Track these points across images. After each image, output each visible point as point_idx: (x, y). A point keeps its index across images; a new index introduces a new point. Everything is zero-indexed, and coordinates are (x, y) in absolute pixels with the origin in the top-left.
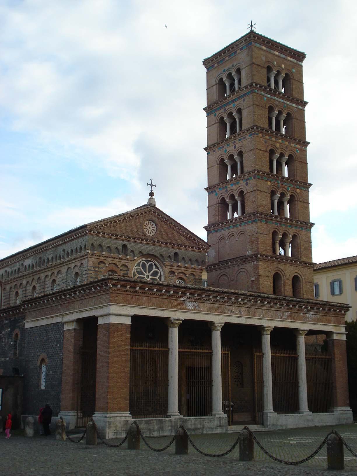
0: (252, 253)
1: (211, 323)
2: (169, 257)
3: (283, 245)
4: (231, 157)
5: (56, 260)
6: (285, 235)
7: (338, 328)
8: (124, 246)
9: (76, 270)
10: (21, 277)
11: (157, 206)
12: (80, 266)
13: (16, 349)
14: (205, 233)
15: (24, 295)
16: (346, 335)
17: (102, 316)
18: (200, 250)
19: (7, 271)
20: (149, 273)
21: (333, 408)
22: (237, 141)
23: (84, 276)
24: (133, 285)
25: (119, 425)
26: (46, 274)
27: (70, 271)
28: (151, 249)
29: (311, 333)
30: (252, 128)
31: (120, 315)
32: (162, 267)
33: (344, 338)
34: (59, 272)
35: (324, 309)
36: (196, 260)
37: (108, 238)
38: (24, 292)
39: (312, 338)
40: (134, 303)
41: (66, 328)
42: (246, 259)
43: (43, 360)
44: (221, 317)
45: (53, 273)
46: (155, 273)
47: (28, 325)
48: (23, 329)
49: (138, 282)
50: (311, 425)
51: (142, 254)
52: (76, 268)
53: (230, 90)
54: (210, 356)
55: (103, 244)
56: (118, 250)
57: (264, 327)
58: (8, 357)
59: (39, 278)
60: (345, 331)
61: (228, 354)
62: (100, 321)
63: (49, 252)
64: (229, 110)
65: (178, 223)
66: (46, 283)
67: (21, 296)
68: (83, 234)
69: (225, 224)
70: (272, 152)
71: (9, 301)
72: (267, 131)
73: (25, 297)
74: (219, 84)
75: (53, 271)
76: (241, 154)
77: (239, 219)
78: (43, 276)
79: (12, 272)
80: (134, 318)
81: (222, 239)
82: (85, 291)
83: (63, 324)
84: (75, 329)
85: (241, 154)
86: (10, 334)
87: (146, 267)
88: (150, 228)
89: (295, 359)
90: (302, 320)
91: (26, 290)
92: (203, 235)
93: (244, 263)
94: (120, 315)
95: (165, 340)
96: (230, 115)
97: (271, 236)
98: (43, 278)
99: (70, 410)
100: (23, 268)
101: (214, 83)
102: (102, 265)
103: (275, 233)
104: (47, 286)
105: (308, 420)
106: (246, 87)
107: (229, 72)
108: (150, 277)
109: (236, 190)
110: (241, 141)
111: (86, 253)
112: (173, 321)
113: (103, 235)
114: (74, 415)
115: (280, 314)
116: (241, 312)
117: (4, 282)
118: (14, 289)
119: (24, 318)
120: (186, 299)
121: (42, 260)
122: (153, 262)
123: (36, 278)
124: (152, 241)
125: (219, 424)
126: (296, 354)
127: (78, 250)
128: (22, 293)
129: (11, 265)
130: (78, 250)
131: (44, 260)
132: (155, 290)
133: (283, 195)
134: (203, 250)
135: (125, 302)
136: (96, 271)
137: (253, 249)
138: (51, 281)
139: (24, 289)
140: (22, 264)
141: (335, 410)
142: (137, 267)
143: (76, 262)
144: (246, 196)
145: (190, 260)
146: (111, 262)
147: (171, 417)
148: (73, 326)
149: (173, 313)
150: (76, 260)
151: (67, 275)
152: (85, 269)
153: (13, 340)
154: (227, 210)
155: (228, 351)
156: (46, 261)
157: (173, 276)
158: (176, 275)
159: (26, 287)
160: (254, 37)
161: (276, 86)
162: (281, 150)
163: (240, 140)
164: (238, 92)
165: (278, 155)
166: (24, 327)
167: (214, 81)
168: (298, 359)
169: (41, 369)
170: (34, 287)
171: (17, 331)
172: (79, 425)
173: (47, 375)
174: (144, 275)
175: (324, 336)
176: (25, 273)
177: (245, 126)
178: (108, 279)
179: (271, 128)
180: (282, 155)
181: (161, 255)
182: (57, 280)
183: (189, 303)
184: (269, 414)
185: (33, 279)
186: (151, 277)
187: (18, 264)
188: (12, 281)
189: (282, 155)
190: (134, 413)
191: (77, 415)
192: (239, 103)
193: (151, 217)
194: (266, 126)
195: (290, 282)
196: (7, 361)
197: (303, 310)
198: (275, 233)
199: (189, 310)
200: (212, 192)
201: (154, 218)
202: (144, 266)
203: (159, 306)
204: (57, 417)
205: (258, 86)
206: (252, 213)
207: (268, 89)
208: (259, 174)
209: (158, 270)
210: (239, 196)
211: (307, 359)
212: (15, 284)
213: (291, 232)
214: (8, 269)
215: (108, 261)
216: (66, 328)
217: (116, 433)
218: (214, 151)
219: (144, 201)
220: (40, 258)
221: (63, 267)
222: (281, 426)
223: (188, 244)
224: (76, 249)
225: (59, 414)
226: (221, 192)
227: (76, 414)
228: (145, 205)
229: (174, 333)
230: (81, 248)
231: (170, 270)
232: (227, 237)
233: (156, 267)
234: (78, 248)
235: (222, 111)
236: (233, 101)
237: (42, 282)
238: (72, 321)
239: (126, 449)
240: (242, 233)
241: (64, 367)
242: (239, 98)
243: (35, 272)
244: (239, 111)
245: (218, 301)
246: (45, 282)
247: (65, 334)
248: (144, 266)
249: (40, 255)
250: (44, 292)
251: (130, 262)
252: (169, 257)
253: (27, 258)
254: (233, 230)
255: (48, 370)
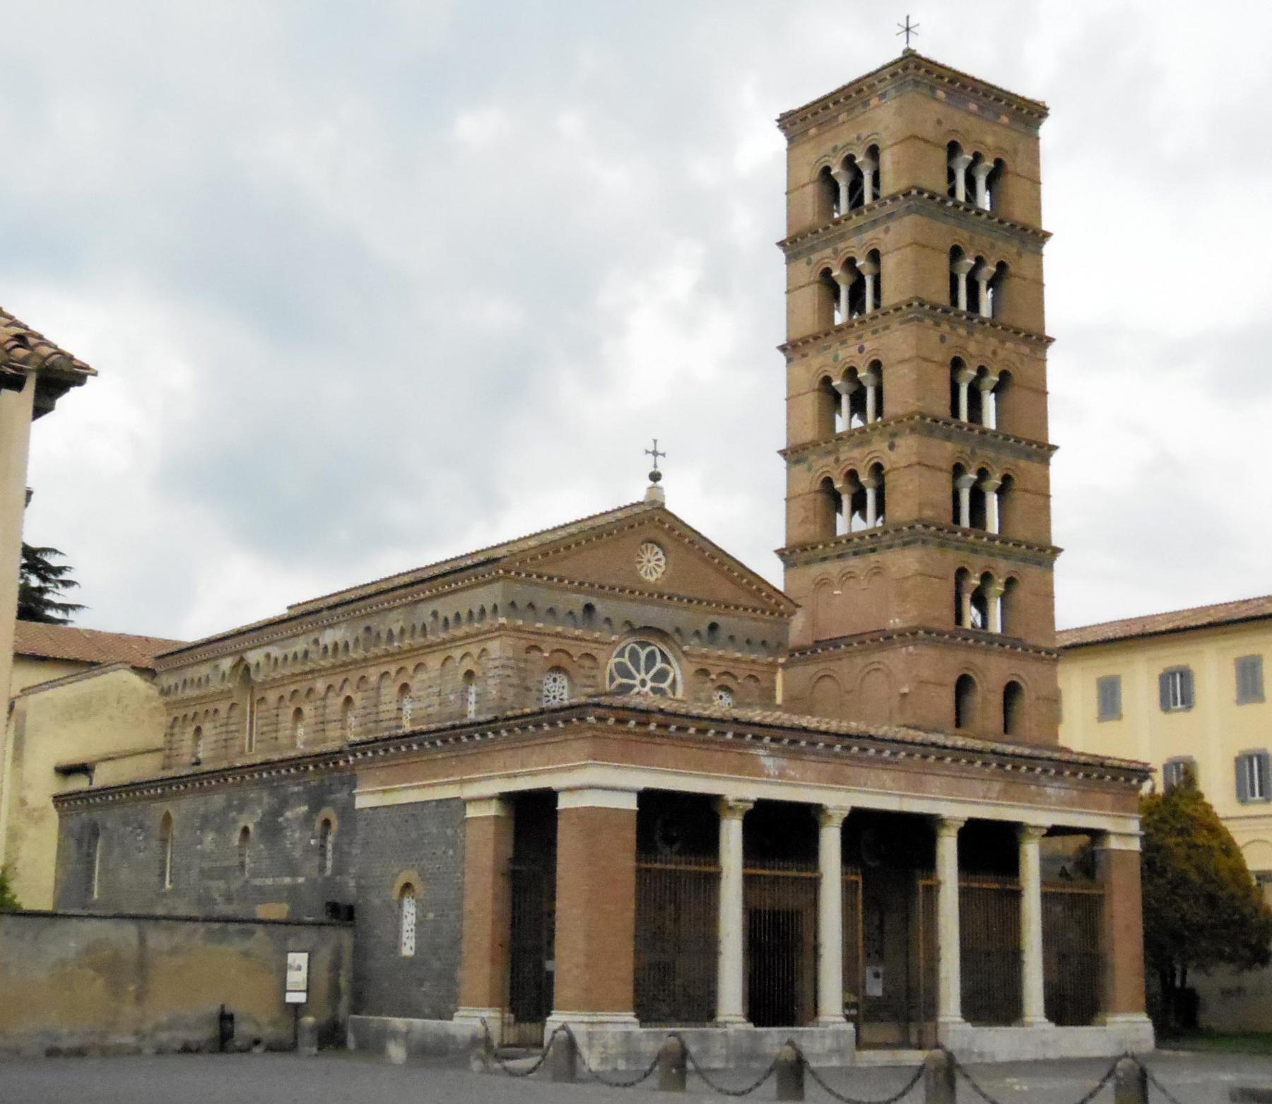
0: (905, 625)
1: (819, 808)
2: (697, 633)
3: (980, 601)
4: (851, 373)
5: (412, 635)
6: (986, 577)
7: (1121, 821)
8: (589, 608)
9: (468, 664)
10: (312, 671)
11: (669, 506)
12: (480, 657)
13: (323, 855)
14: (779, 565)
15: (321, 719)
16: (1143, 839)
17: (569, 790)
18: (772, 618)
19: (273, 656)
20: (647, 672)
21: (1107, 1016)
22: (867, 335)
23: (491, 682)
24: (643, 718)
25: (611, 1042)
26: (383, 669)
27: (449, 663)
28: (652, 614)
29: (1055, 831)
30: (909, 305)
31: (613, 789)
32: (678, 660)
33: (1135, 845)
34: (419, 667)
35: (1087, 776)
36: (764, 643)
37: (550, 588)
38: (320, 711)
39: (1057, 843)
40: (644, 762)
41: (471, 812)
42: (888, 638)
43: (407, 887)
44: (842, 794)
45: (401, 670)
46: (661, 675)
47: (364, 800)
48: (348, 812)
49: (653, 712)
50: (1051, 1054)
51: (632, 629)
52: (468, 659)
53: (851, 196)
54: (814, 885)
55: (538, 604)
56: (574, 618)
57: (942, 820)
58: (302, 876)
59: (363, 677)
60: (1138, 828)
61: (857, 882)
62: (563, 803)
63: (394, 615)
64: (846, 250)
65: (721, 550)
66: (383, 691)
67: (312, 721)
68: (490, 578)
69: (832, 545)
70: (957, 365)
71: (276, 731)
72: (945, 311)
73: (323, 723)
74: (818, 180)
75: (402, 664)
76: (876, 367)
77: (872, 536)
78: (373, 674)
79: (286, 658)
80: (648, 798)
81: (823, 583)
82: (524, 728)
83: (464, 803)
84: (496, 817)
85: (876, 367)
86: (307, 820)
87: (639, 659)
88: (649, 561)
89: (1016, 895)
90: (1033, 802)
91: (325, 707)
92: (773, 573)
93: (881, 647)
94: (613, 789)
95: (709, 845)
96: (850, 264)
97: (952, 580)
98: (373, 679)
99: (483, 1006)
100: (318, 651)
101: (806, 180)
102: (535, 655)
103: (961, 573)
104: (383, 699)
105: (1044, 1044)
106: (894, 198)
107: (846, 154)
108: (649, 684)
109: (862, 461)
110: (877, 335)
111: (497, 626)
112: (731, 804)
113: (539, 581)
114: (496, 1018)
115: (980, 787)
116: (889, 783)
117: (263, 683)
118: (291, 700)
119: (352, 783)
120: (761, 752)
121: (374, 634)
122: (657, 646)
123: (354, 676)
124: (656, 596)
125: (835, 1045)
126: (1018, 884)
127: (476, 616)
128: (313, 713)
129: (282, 640)
130: (476, 616)
131: (378, 634)
132: (692, 731)
133: (983, 474)
134: (781, 614)
135: (624, 757)
136: (519, 669)
137: (904, 612)
138: (397, 689)
139: (318, 703)
140: (316, 642)
141: (1109, 1019)
142: (617, 660)
143: (468, 646)
144: (890, 479)
145: (748, 642)
146: (557, 647)
147: (726, 1027)
148: (489, 808)
149: (732, 784)
150: (469, 641)
151: (441, 676)
152: (491, 664)
153: (318, 833)
154: (838, 507)
155: (857, 874)
156: (384, 636)
157: (706, 682)
158: (712, 680)
159: (324, 698)
160: (917, 68)
161: (969, 194)
162: (980, 359)
163: (875, 332)
164: (870, 209)
165: (971, 373)
166: (354, 805)
167: (809, 173)
168: (1023, 896)
169: (401, 906)
170: (348, 700)
171: (328, 812)
172: (505, 1043)
173: (420, 924)
174: (633, 678)
175: (1085, 839)
176: (323, 663)
177: (888, 299)
178: (586, 705)
179: (954, 301)
180: (982, 371)
181: (678, 630)
182: (415, 685)
183: (769, 763)
184: (951, 1027)
185: (346, 680)
186: (653, 684)
187: (302, 639)
188: (286, 682)
189: (982, 371)
190: (646, 1014)
191: (503, 1018)
192: (871, 237)
193: (654, 534)
194: (944, 299)
195: (998, 699)
196: (301, 885)
197: (1038, 777)
198: (961, 573)
199: (768, 776)
200: (797, 462)
201: (664, 539)
202: (634, 656)
203: (699, 766)
204: (449, 1022)
205: (926, 195)
206: (904, 523)
207: (950, 204)
208: (926, 425)
209: (669, 667)
210: (870, 475)
211: (1045, 897)
212: (293, 688)
213: (1002, 569)
214: (275, 651)
215: (548, 645)
216: (471, 812)
217: (604, 1060)
218: (804, 356)
219: (637, 492)
220: (368, 629)
221: (431, 656)
222: (981, 1055)
223: (743, 601)
224: (471, 613)
225: (456, 1014)
226: (823, 465)
227: (498, 1015)
228: (639, 504)
229: (732, 834)
230: (483, 611)
231: (699, 667)
232: (836, 581)
233: (665, 658)
234: (476, 611)
235: (828, 252)
236: (859, 230)
237: (372, 689)
238: (491, 798)
239: (654, 1090)
240: (878, 571)
241: (469, 905)
242: (875, 223)
243: (351, 663)
244: (875, 256)
245: (836, 755)
246: (379, 688)
247: (468, 830)
248: (634, 656)
249: (368, 622)
250: (377, 713)
251: (601, 646)
252: (697, 633)
253: (331, 626)
254: (853, 563)
255: (422, 907)
